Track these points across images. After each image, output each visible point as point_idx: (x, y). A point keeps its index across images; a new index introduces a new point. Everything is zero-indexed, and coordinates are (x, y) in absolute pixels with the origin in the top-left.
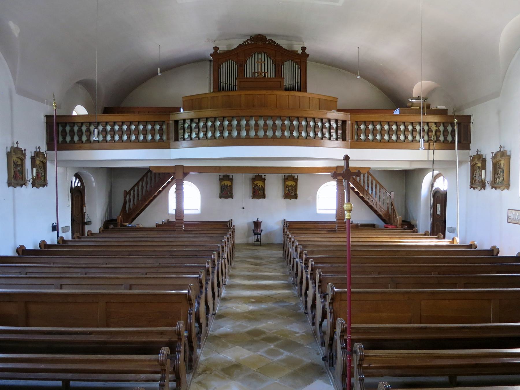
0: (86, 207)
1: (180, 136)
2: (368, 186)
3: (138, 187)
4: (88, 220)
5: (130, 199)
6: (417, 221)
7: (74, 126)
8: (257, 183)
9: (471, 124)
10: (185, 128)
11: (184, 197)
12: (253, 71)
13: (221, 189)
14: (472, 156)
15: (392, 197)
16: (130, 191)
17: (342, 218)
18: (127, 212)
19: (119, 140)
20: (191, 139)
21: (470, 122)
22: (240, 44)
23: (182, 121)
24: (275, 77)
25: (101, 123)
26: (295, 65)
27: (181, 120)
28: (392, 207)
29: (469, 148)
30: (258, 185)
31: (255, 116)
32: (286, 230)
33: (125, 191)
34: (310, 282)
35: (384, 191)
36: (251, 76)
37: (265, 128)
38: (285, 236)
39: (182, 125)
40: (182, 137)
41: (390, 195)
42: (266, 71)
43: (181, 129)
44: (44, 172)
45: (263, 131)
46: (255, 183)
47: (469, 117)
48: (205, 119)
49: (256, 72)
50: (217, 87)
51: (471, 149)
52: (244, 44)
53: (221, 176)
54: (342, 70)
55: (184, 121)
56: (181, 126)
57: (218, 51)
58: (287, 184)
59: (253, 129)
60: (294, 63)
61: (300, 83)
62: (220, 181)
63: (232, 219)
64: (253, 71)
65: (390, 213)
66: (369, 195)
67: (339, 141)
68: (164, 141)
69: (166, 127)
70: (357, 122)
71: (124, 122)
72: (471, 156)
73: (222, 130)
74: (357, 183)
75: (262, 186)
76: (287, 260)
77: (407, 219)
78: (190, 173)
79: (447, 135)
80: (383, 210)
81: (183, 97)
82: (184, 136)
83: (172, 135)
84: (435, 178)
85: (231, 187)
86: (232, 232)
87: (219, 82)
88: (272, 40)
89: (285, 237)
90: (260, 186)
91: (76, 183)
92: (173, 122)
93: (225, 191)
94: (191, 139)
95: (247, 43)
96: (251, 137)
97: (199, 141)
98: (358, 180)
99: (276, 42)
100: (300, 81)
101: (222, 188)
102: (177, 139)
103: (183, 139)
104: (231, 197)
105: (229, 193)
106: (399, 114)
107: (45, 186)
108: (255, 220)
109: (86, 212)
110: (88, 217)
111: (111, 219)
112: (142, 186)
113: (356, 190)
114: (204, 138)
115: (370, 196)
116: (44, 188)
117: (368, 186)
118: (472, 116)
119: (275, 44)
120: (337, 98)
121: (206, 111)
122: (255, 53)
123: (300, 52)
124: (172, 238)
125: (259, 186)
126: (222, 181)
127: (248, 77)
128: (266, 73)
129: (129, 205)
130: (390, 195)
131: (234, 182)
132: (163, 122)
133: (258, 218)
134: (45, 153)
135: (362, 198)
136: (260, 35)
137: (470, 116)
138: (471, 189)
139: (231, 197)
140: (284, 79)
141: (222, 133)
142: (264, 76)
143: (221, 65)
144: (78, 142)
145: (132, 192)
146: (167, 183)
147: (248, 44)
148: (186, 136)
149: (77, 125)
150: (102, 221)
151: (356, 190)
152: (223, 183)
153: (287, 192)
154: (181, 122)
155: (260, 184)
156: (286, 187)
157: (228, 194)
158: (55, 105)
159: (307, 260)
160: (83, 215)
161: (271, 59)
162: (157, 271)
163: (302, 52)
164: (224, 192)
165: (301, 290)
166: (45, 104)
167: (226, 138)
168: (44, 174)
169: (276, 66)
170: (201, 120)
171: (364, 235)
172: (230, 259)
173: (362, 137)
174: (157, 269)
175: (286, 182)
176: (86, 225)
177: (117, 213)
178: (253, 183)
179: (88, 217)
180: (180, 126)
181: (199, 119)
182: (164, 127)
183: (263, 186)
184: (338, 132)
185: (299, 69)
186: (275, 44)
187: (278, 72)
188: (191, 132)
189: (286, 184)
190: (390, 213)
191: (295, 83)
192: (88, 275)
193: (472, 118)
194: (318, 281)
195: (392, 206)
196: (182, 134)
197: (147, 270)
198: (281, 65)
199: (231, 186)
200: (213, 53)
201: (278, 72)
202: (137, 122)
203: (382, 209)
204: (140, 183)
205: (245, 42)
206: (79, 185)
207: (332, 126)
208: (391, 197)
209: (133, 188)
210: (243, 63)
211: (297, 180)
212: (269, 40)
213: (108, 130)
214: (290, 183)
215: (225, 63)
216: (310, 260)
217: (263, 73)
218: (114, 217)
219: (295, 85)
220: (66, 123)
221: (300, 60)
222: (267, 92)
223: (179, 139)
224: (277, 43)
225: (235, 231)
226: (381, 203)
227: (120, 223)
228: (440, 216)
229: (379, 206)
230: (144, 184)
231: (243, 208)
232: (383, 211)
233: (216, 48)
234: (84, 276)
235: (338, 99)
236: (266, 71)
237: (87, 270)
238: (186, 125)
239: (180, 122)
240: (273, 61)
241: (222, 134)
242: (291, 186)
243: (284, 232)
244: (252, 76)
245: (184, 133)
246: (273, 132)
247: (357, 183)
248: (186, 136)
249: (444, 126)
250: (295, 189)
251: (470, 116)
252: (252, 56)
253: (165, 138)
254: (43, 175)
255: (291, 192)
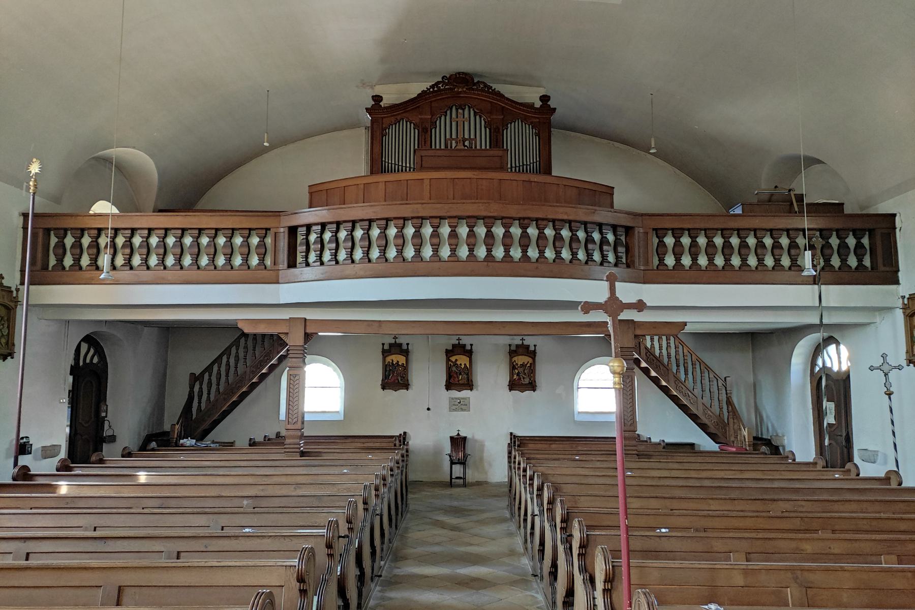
0: (107, 406)
1: (300, 259)
2: (678, 366)
3: (219, 367)
4: (110, 433)
5: (201, 389)
6: (785, 438)
7: (82, 236)
8: (456, 360)
9: (897, 230)
10: (310, 242)
11: (304, 387)
12: (448, 136)
13: (386, 371)
14: (907, 296)
15: (728, 389)
16: (203, 373)
17: (632, 428)
18: (194, 417)
19: (173, 265)
20: (322, 264)
21: (895, 228)
22: (424, 90)
23: (305, 229)
24: (490, 147)
25: (139, 232)
26: (528, 130)
27: (302, 226)
28: (730, 409)
29: (896, 282)
30: (458, 363)
31: (450, 217)
32: (513, 453)
33: (192, 374)
34: (579, 579)
35: (711, 376)
36: (443, 147)
37: (469, 241)
38: (513, 466)
39: (304, 237)
40: (303, 261)
41: (725, 384)
42: (472, 137)
43: (301, 244)
44: (8, 327)
45: (467, 247)
46: (453, 359)
47: (891, 218)
48: (350, 224)
49: (453, 139)
50: (377, 165)
51: (901, 282)
52: (431, 90)
53: (385, 346)
54: (617, 144)
55: (309, 227)
56: (302, 237)
57: (382, 104)
58: (515, 361)
59: (447, 243)
60: (527, 126)
61: (538, 163)
62: (383, 355)
63: (406, 431)
64: (448, 136)
65: (726, 421)
66: (681, 384)
67: (620, 267)
68: (268, 268)
69: (271, 241)
70: (656, 230)
71: (187, 229)
72: (903, 297)
73: (384, 245)
74: (655, 358)
75: (465, 364)
76: (517, 517)
77: (762, 434)
78: (320, 334)
79: (848, 255)
80: (711, 414)
81: (309, 186)
82: (307, 257)
83: (283, 256)
84: (818, 350)
85: (406, 368)
86: (403, 456)
87: (382, 161)
88: (484, 82)
89: (512, 468)
90: (463, 366)
91: (89, 356)
92: (286, 230)
93: (393, 375)
94: (322, 264)
95: (436, 89)
96: (442, 259)
97: (337, 266)
98: (656, 354)
99: (492, 87)
100: (538, 159)
101: (388, 369)
102: (292, 264)
103: (304, 265)
104: (406, 386)
105: (401, 380)
106: (741, 213)
107: (9, 358)
108: (454, 434)
109: (106, 417)
110: (110, 427)
111: (161, 431)
112: (228, 364)
113: (653, 374)
114: (347, 262)
115: (683, 386)
116: (6, 361)
117: (678, 366)
118: (898, 215)
119: (490, 90)
120: (614, 188)
121: (351, 207)
122: (452, 107)
123: (538, 104)
124: (273, 469)
125: (461, 364)
126: (388, 356)
127: (438, 147)
128: (472, 139)
129: (200, 403)
130: (725, 384)
131: (410, 357)
132: (267, 229)
133: (459, 431)
134: (13, 289)
135: (665, 390)
136: (463, 73)
137: (894, 215)
138: (908, 365)
139: (406, 386)
140: (508, 150)
141: (385, 250)
142: (468, 145)
143: (387, 131)
144: (88, 268)
145: (206, 376)
146: (278, 358)
147: (439, 90)
148: (312, 257)
149: (88, 234)
150: (139, 434)
151: (653, 374)
152: (389, 359)
153: (515, 377)
154: (302, 231)
155: (462, 360)
156: (513, 367)
157: (398, 381)
158: (36, 184)
159: (566, 520)
160: (100, 422)
161: (482, 119)
162: (206, 547)
163: (541, 105)
164: (390, 377)
165: (554, 592)
166: (24, 191)
167: (392, 261)
168: (9, 333)
169: (492, 131)
170: (342, 226)
171: (682, 464)
172: (397, 514)
173: (670, 261)
174: (206, 541)
175: (512, 358)
176: (105, 442)
177: (171, 420)
178: (448, 360)
179: (110, 427)
180: (300, 238)
181: (338, 224)
182: (269, 241)
183: (468, 366)
184: (619, 251)
185: (536, 136)
186: (490, 90)
187: (496, 141)
188: (322, 250)
189: (513, 361)
190: (726, 421)
191: (528, 163)
192: (32, 562)
193: (897, 219)
194: (603, 578)
195: (730, 406)
196: (304, 254)
197: (181, 546)
198: (501, 131)
199: (405, 365)
200: (372, 107)
201: (496, 141)
202: (212, 229)
203: (709, 412)
204: (225, 359)
205: (432, 86)
206: (95, 360)
207: (606, 238)
208: (726, 388)
209: (209, 369)
210: (430, 126)
211: (534, 352)
212: (478, 82)
213: (152, 245)
214: (521, 360)
215: (394, 126)
216: (577, 520)
217: (466, 140)
218: (167, 427)
219: (528, 167)
220: (66, 230)
221: (538, 120)
222: (474, 175)
223: (298, 265)
224: (493, 88)
225: (409, 454)
226: (706, 400)
227: (175, 439)
228: (835, 427)
229: (701, 407)
230: (232, 361)
231: (428, 409)
232: (711, 416)
233: (377, 99)
234: (23, 563)
235: (615, 189)
236: (472, 137)
237: (32, 546)
238: (313, 237)
239: (299, 229)
240: (485, 122)
241: (385, 253)
242: (523, 365)
243: (509, 457)
244: (446, 146)
245: (308, 251)
246: (487, 249)
247: (655, 358)
248: (312, 257)
249: (838, 237)
250: (531, 370)
251: (894, 215)
252: (446, 112)
253: (268, 262)
254: (5, 334)
255: (524, 378)
